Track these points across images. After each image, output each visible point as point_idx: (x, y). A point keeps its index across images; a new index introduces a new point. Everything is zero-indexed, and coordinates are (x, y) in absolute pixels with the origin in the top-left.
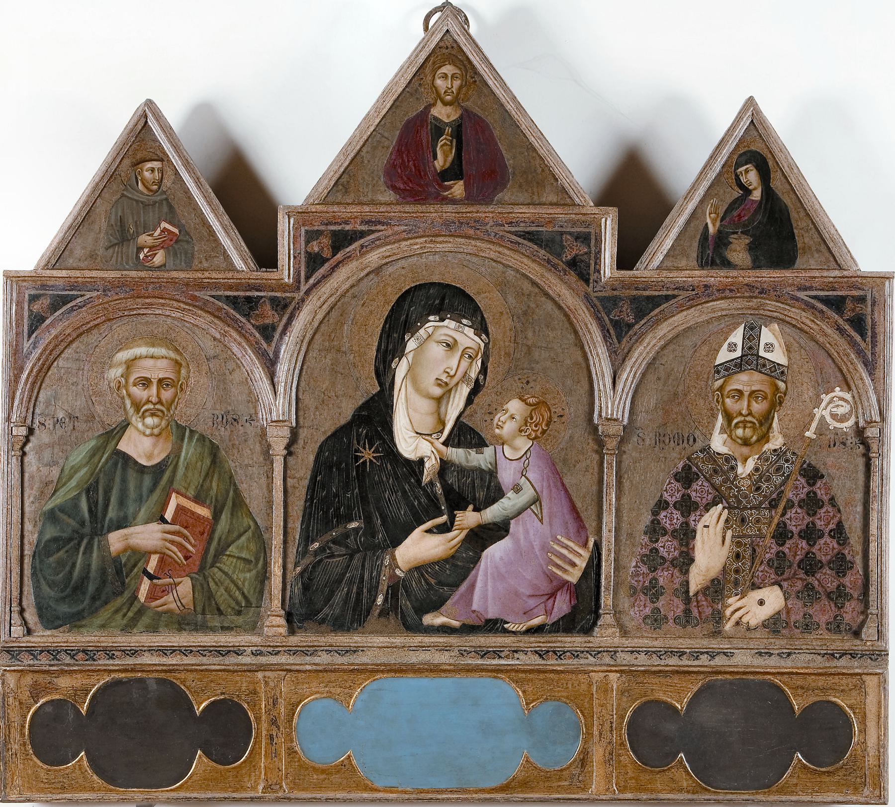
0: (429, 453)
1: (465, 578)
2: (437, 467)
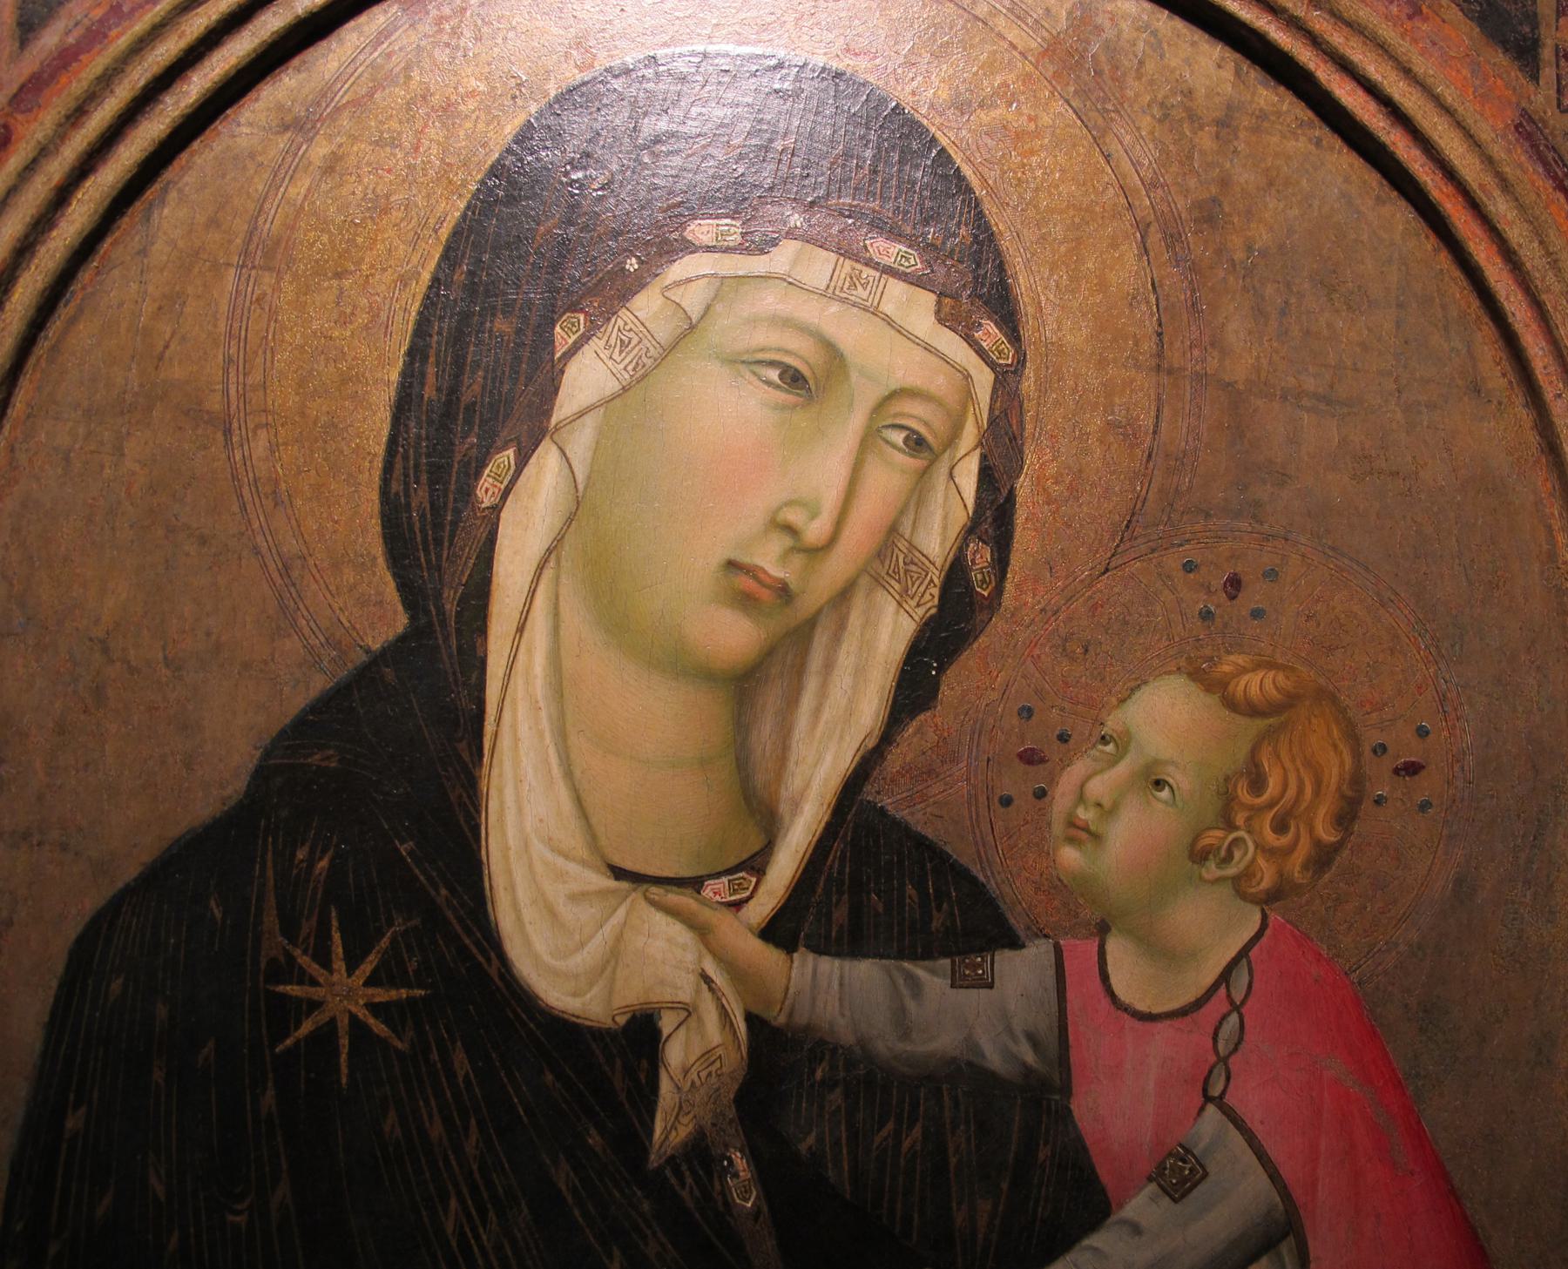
0: (684, 988)
2: (734, 1060)
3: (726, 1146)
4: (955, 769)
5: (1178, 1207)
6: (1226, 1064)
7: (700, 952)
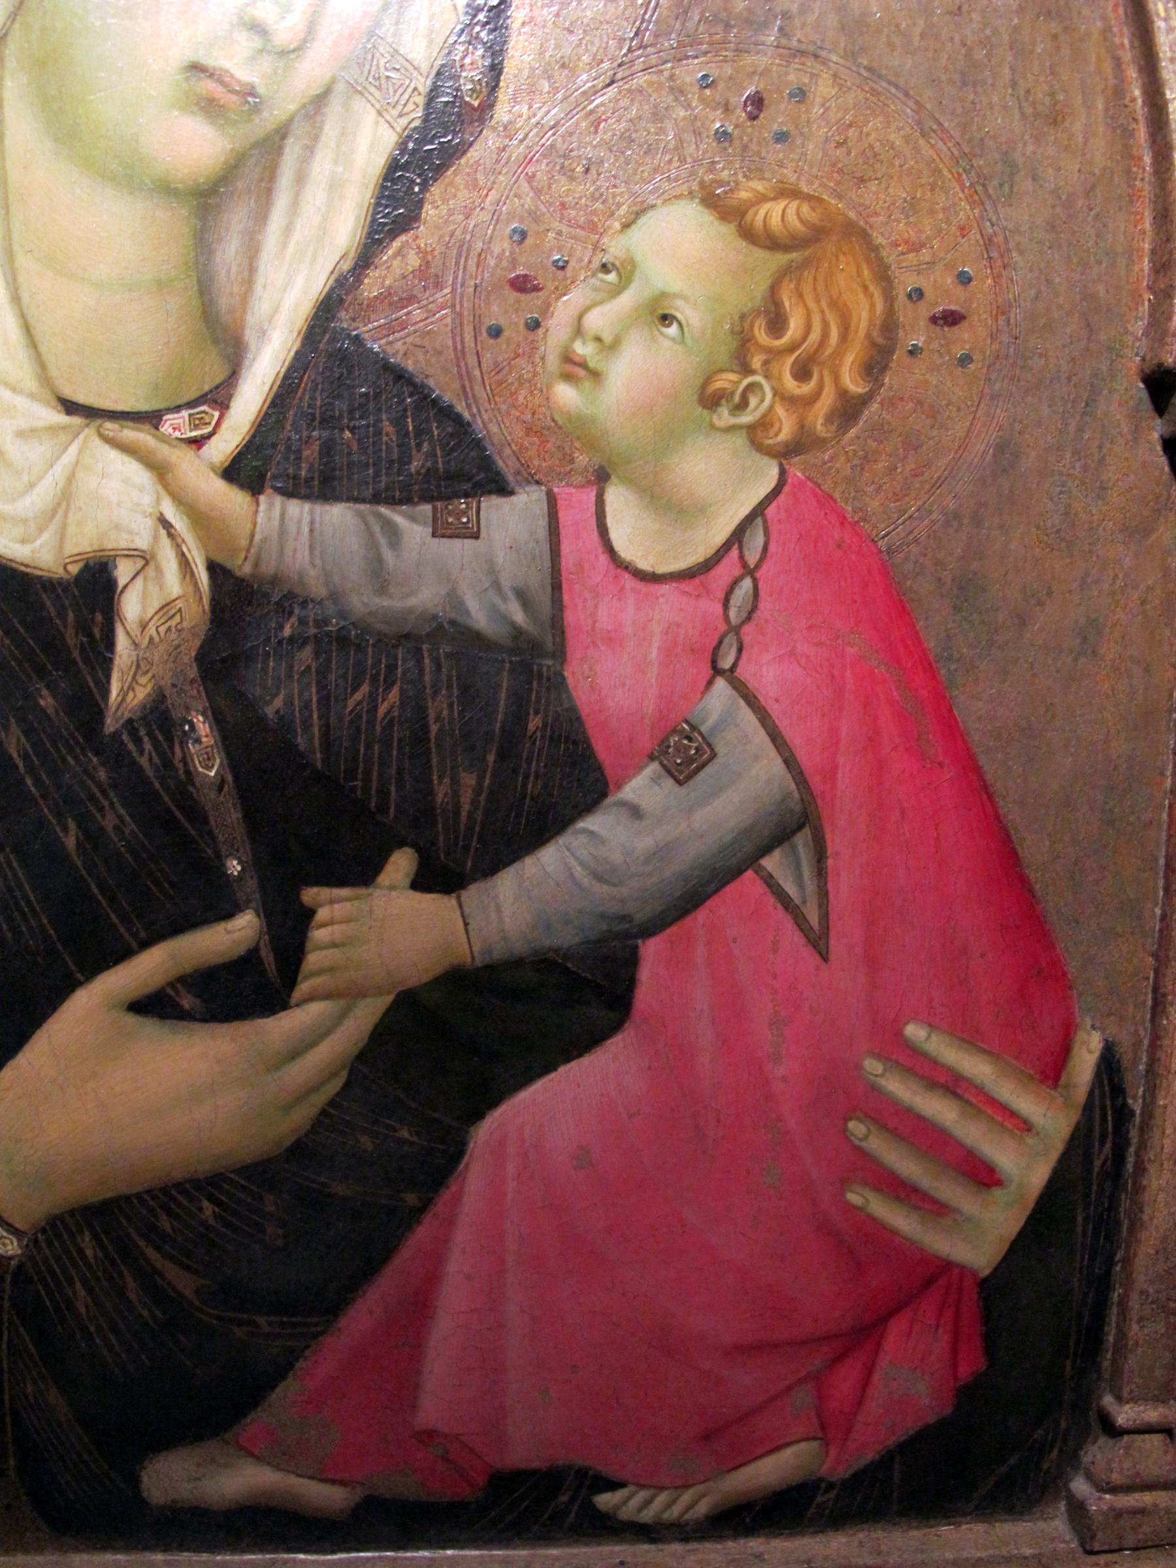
0: (141, 535)
1: (370, 1268)
3: (188, 709)
4: (438, 295)
5: (682, 791)
6: (737, 634)
7: (158, 493)
